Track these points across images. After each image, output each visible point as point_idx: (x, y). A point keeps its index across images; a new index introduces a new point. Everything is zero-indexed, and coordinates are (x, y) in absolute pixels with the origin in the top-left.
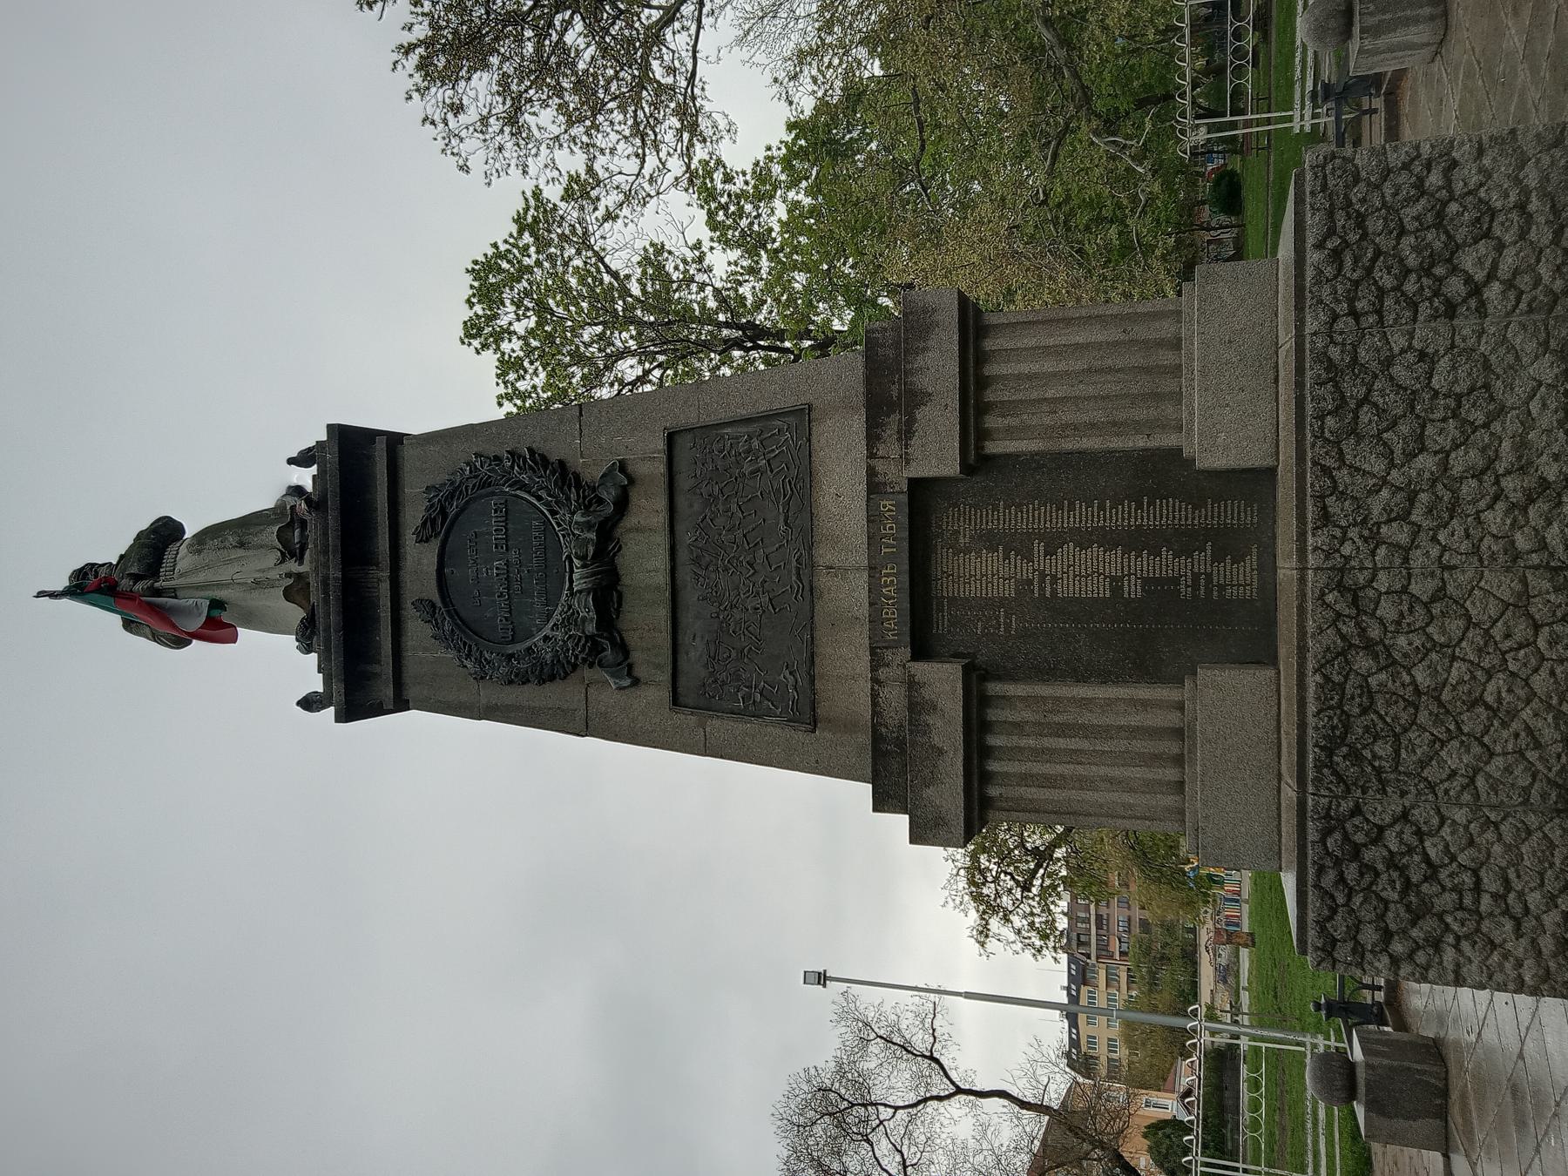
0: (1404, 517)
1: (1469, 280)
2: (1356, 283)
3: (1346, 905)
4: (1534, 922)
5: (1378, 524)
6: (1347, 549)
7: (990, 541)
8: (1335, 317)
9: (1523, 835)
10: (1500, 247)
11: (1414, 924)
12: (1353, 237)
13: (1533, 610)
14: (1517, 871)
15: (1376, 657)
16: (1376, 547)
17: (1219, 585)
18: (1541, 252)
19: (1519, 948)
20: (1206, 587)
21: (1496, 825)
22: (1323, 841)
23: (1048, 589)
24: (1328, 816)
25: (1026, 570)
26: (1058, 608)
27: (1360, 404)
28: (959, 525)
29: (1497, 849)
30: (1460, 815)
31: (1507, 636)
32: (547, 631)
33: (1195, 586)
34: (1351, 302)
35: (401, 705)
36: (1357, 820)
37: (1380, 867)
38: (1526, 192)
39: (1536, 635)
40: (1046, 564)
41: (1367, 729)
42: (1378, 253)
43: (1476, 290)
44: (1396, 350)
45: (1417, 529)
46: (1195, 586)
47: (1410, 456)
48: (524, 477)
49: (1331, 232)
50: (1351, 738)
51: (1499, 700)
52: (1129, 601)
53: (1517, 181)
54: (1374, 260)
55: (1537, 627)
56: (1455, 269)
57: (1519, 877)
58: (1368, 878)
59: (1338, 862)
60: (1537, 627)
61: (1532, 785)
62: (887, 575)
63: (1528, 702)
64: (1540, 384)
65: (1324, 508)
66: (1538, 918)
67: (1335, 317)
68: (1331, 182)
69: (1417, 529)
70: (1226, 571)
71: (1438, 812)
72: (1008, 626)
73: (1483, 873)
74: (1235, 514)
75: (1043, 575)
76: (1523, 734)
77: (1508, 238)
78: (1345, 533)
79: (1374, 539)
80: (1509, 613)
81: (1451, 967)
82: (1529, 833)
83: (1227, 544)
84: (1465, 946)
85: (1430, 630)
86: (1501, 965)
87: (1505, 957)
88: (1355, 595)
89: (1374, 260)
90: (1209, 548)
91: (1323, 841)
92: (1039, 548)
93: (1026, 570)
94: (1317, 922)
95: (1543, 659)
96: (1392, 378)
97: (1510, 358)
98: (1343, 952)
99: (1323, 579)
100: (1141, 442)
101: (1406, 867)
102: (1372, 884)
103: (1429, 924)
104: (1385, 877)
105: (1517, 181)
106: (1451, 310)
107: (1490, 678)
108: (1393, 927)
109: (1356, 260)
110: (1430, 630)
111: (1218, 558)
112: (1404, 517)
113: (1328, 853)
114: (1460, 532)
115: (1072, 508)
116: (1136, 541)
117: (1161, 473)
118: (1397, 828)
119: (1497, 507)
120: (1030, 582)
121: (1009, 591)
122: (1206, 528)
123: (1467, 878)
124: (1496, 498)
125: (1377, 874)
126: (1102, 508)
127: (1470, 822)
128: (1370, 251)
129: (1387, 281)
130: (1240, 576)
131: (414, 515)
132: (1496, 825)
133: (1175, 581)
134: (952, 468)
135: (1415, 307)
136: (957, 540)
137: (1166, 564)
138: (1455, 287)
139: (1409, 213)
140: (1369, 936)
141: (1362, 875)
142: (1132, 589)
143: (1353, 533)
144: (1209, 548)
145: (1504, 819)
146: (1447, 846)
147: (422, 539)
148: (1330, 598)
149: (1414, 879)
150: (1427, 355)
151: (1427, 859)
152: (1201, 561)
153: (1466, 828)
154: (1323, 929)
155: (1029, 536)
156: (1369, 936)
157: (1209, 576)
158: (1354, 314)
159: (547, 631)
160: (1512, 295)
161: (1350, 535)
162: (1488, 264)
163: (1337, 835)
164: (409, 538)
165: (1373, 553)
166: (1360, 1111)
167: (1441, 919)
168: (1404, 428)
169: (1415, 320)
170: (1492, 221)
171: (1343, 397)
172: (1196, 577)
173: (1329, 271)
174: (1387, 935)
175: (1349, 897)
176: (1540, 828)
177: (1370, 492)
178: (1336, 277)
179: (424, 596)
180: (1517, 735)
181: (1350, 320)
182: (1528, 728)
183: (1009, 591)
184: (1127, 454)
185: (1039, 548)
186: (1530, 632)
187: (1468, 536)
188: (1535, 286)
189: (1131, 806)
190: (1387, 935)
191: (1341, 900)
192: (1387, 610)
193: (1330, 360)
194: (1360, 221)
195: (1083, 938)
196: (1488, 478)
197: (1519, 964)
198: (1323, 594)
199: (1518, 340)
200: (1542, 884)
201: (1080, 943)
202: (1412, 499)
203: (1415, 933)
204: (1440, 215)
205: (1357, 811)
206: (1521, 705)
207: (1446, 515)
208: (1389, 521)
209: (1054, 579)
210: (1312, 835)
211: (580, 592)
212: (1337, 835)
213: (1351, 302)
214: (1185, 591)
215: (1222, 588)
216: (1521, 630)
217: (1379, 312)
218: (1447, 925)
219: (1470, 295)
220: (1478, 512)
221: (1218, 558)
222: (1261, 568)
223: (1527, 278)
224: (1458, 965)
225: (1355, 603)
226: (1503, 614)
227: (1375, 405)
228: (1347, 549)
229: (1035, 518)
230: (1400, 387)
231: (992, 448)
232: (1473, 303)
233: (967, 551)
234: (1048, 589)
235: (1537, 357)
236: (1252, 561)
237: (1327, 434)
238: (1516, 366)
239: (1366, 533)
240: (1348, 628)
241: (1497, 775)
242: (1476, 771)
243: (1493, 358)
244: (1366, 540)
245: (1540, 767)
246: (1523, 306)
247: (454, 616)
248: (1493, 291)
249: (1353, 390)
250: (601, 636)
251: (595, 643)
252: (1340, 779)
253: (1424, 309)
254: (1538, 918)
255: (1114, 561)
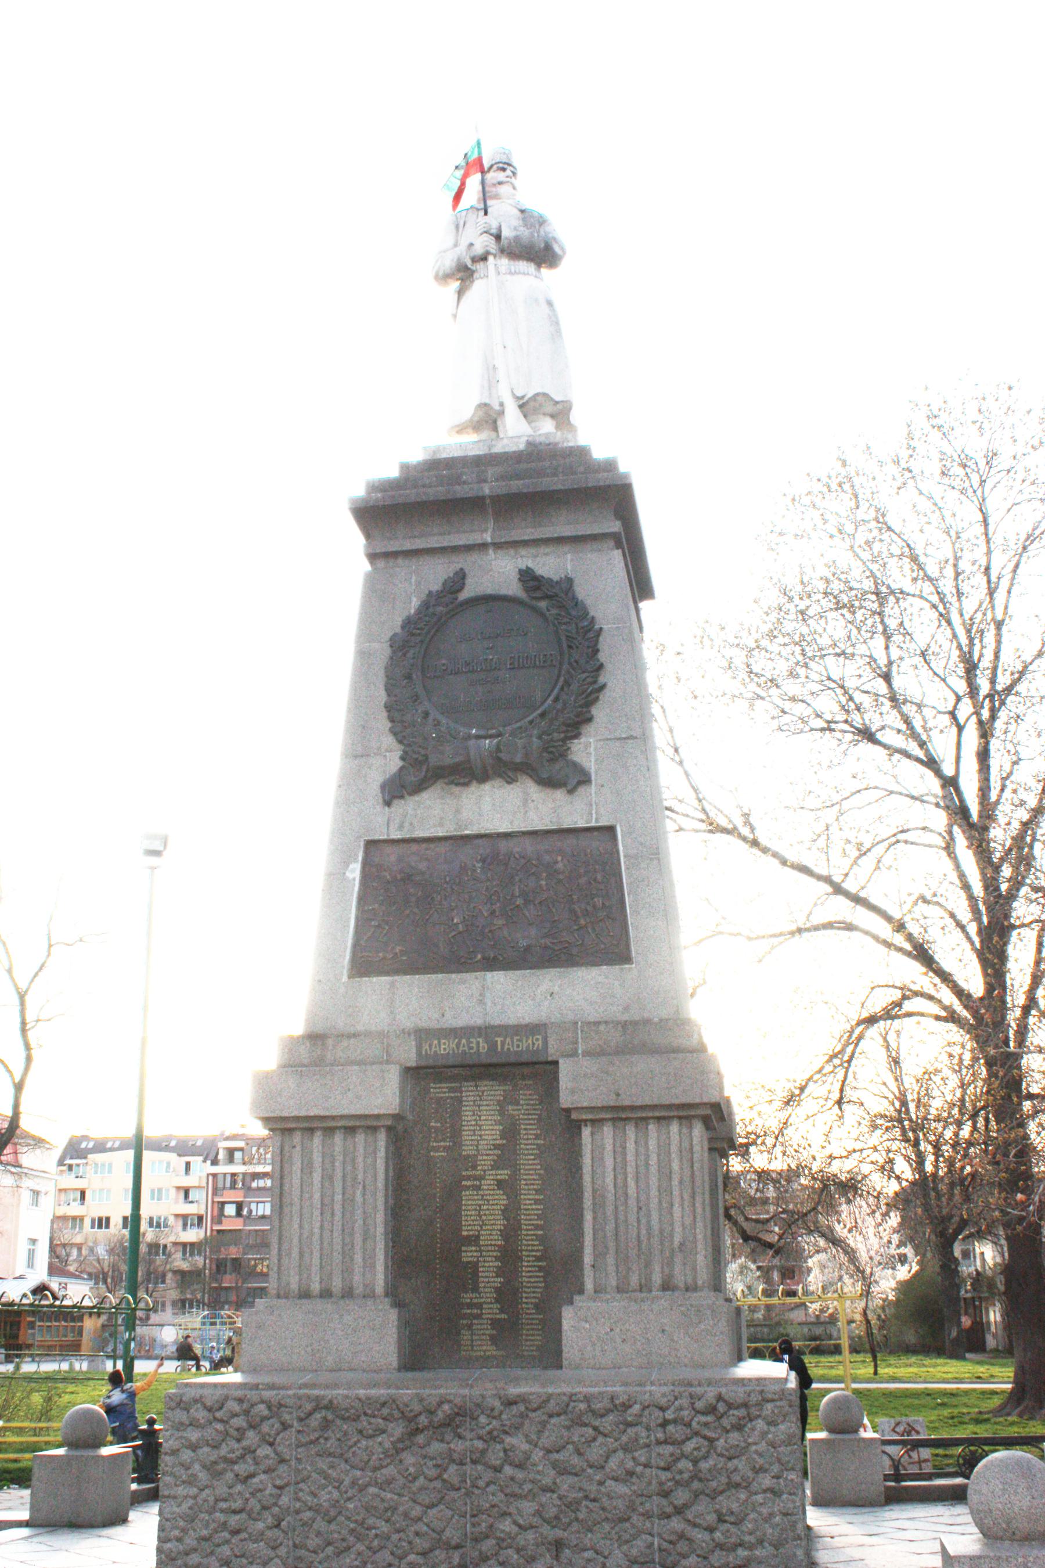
0: (507, 1460)
1: (686, 1506)
2: (688, 1425)
3: (215, 1419)
4: (209, 1551)
5: (502, 1442)
6: (483, 1419)
7: (511, 1132)
8: (662, 1409)
9: (272, 1544)
10: (711, 1530)
11: (204, 1467)
12: (725, 1422)
13: (437, 1552)
14: (245, 1539)
15: (400, 1440)
16: (485, 1441)
17: (472, 1324)
18: (705, 1558)
19: (190, 1541)
20: (471, 1314)
21: (278, 1526)
22: (263, 1402)
23: (469, 1183)
24: (280, 1405)
25: (485, 1162)
26: (453, 1191)
27: (595, 1429)
28: (526, 1105)
29: (260, 1525)
30: (284, 1500)
31: (417, 1534)
32: (434, 714)
33: (470, 1306)
34: (675, 1421)
35: (372, 557)
36: (277, 1426)
37: (245, 1443)
38: (751, 1547)
39: (418, 1554)
40: (488, 1182)
41: (345, 1434)
42: (711, 1441)
43: (679, 1511)
44: (636, 1454)
45: (498, 1470)
46: (470, 1306)
47: (554, 1465)
48: (574, 687)
49: (730, 1406)
50: (339, 1422)
51: (369, 1529)
52: (460, 1251)
53: (761, 1542)
54: (705, 1437)
55: (424, 1554)
56: (696, 1495)
57: (241, 1540)
58: (235, 1434)
59: (247, 1412)
60: (424, 1554)
61: (308, 1550)
62: (478, 1043)
63: (369, 1548)
64: (605, 1557)
65: (516, 1403)
66: (212, 1553)
67: (662, 1409)
68: (769, 1406)
69: (498, 1470)
70: (483, 1328)
71: (287, 1485)
72: (436, 1149)
73: (244, 1515)
74: (532, 1340)
75: (481, 1178)
76: (344, 1544)
77: (718, 1535)
78: (494, 1418)
79: (492, 1438)
80: (435, 1535)
81: (173, 1493)
82: (274, 1548)
83: (506, 1331)
84: (191, 1502)
85: (422, 1479)
86: (176, 1528)
87: (184, 1530)
88: (449, 1423)
89: (705, 1437)
90: (503, 1316)
91: (263, 1402)
92: (504, 1174)
93: (485, 1162)
94: (201, 1397)
95: (401, 1558)
96: (615, 1451)
97: (627, 1537)
98: (181, 1416)
99: (458, 1401)
100: (588, 1259)
101: (245, 1462)
102: (231, 1436)
103: (203, 1476)
104: (236, 1446)
105: (761, 1542)
106: (666, 1494)
107: (387, 1521)
108: (200, 1451)
109: (706, 1424)
110: (422, 1479)
111: (495, 1323)
112: (507, 1460)
113: (252, 1405)
114: (496, 1500)
115: (537, 1202)
116: (509, 1256)
117: (563, 1275)
118: (273, 1455)
119: (513, 1527)
120: (474, 1167)
121: (468, 1150)
122: (518, 1314)
123: (238, 1505)
124: (520, 1526)
125: (238, 1441)
126: (537, 1227)
127: (279, 1507)
128: (713, 1435)
129: (689, 1446)
130: (478, 1340)
131: (549, 565)
132: (278, 1526)
133: (475, 1289)
134: (566, 1100)
135: (666, 1469)
136: (511, 1103)
137: (489, 1277)
138: (681, 1496)
139: (740, 1464)
140: (194, 1435)
141: (238, 1430)
142: (469, 1254)
143: (495, 1423)
144: (503, 1316)
145: (283, 1531)
146: (260, 1490)
147: (527, 577)
148: (446, 1407)
149: (236, 1467)
150: (631, 1476)
151: (252, 1476)
152: (492, 1310)
153: (275, 1504)
154: (196, 1401)
155: (515, 1168)
156: (194, 1435)
157: (479, 1316)
158: (664, 1424)
159: (434, 714)
160: (673, 1538)
161: (494, 1422)
162: (698, 1521)
163: (266, 1412)
164: (527, 559)
165: (480, 1438)
166: (61, 1451)
167: (207, 1487)
168: (576, 1460)
169: (658, 1468)
170: (732, 1523)
171: (602, 1416)
172: (480, 1306)
173: (700, 1405)
174: (194, 1447)
175: (222, 1421)
176: (277, 1556)
177: (527, 1436)
178: (694, 1409)
179: (469, 581)
180: (343, 1540)
181: (660, 1421)
182: (348, 1548)
183: (468, 1150)
184: (580, 1250)
185: (504, 1174)
186: (420, 1550)
187: (493, 1506)
188: (679, 1554)
189: (289, 1254)
190: (194, 1447)
191: (218, 1415)
192: (436, 1447)
193: (631, 1406)
194: (739, 1427)
195: (238, 1155)
196: (536, 1521)
197: (179, 1540)
198: (449, 1402)
199: (639, 1543)
200: (237, 1556)
201: (231, 1152)
202: (520, 1466)
203: (197, 1467)
204: (737, 1485)
205: (285, 1426)
206: (367, 1543)
207: (508, 1491)
208: (505, 1451)
209: (478, 1188)
210: (267, 1394)
211: (466, 748)
212: (266, 1412)
213: (675, 1421)
214: (467, 1297)
215: (470, 1327)
216: (421, 1544)
217: (665, 1442)
218: (203, 1490)
219: (675, 1507)
220: (510, 1514)
221: (495, 1323)
222: (487, 1358)
223: (686, 1548)
224: (175, 1497)
225: (442, 1425)
226: (433, 1530)
227: (594, 1439)
228: (483, 1419)
229: (530, 1167)
230: (608, 1458)
231: (586, 1132)
232: (669, 1510)
233: (502, 1112)
234: (469, 1183)
235: (626, 1556)
236: (491, 1350)
237: (572, 1404)
238: (622, 1542)
239: (495, 1433)
240: (423, 1420)
241: (315, 1526)
242: (317, 1511)
243: (627, 1525)
244: (490, 1433)
245: (322, 1555)
246: (665, 1545)
247: (445, 608)
248: (676, 1524)
249: (607, 1423)
250: (428, 770)
251: (421, 763)
252: (310, 1414)
253: (664, 1476)
254: (212, 1553)
255: (492, 1237)
